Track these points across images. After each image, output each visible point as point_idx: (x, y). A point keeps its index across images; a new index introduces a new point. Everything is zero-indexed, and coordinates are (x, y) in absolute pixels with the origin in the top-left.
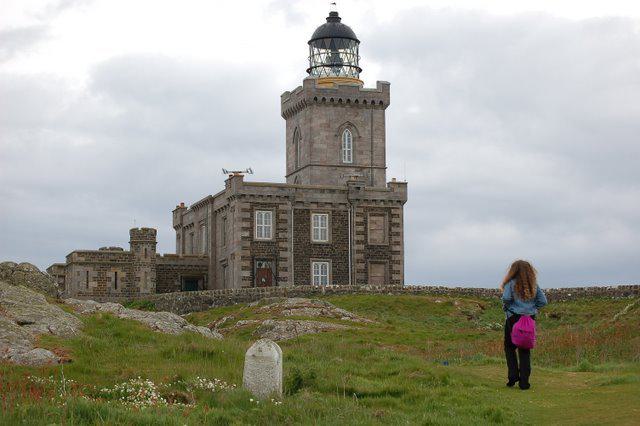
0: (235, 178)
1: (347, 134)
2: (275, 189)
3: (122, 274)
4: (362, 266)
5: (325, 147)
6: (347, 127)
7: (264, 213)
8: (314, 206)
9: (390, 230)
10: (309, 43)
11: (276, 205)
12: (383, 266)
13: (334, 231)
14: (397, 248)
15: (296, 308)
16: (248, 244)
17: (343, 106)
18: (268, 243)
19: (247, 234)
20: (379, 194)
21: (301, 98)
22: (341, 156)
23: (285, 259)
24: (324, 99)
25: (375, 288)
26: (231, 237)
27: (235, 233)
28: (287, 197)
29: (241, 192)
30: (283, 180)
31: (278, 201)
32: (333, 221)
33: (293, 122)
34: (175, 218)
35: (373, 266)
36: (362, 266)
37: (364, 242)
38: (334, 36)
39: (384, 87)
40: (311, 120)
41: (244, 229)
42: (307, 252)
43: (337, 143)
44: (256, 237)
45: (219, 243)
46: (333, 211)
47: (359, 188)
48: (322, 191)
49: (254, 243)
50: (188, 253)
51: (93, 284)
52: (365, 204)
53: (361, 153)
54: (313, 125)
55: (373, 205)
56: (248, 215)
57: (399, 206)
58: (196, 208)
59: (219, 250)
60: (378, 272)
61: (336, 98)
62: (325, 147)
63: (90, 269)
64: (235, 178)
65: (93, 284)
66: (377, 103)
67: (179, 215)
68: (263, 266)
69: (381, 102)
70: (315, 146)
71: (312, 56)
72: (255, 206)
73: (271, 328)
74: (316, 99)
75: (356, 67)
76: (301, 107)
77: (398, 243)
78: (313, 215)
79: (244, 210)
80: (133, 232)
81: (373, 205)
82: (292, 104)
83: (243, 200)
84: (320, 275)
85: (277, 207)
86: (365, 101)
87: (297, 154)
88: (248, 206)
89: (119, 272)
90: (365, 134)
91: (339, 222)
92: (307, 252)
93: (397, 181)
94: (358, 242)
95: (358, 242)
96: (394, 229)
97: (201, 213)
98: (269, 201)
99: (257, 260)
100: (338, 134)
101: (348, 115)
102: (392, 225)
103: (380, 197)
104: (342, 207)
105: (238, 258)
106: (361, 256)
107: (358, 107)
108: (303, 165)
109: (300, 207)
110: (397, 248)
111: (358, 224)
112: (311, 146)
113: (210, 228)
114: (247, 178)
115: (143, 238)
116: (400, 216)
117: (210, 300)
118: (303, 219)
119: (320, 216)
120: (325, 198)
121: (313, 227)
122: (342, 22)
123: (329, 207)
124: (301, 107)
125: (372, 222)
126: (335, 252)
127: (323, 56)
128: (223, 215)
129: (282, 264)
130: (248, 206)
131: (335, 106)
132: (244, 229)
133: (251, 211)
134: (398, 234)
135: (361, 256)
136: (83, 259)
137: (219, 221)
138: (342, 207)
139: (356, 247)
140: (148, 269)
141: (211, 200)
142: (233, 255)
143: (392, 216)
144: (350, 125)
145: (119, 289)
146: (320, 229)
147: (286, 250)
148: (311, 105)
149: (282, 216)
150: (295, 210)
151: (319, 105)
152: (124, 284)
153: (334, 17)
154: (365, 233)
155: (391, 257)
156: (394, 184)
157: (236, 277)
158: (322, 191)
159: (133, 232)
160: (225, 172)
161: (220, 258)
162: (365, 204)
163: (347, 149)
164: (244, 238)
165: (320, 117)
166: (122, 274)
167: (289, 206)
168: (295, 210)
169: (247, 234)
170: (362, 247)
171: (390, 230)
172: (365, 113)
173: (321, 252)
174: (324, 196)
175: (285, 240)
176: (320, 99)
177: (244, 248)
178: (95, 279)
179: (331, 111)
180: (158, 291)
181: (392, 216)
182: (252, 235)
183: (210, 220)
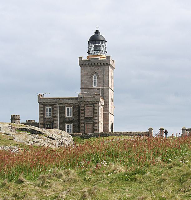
2: (52, 100)
4: (83, 125)
5: (86, 81)
9: (94, 111)
10: (88, 42)
11: (53, 105)
12: (91, 125)
14: (97, 118)
16: (43, 119)
20: (89, 99)
31: (53, 104)
36: (83, 125)
38: (96, 39)
43: (91, 80)
44: (46, 116)
47: (82, 97)
49: (44, 118)
52: (85, 103)
53: (100, 83)
55: (87, 103)
56: (43, 109)
60: (90, 126)
66: (105, 64)
69: (107, 63)
72: (45, 106)
77: (96, 116)
78: (66, 108)
81: (87, 103)
84: (69, 129)
86: (104, 63)
88: (43, 106)
91: (76, 109)
94: (82, 116)
95: (82, 116)
96: (95, 111)
98: (50, 104)
100: (91, 76)
102: (94, 110)
104: (77, 104)
107: (98, 66)
110: (97, 118)
111: (82, 110)
114: (45, 96)
118: (62, 109)
126: (74, 120)
133: (44, 108)
134: (97, 113)
138: (77, 104)
139: (57, 122)
143: (95, 106)
147: (56, 120)
149: (55, 109)
155: (94, 121)
162: (85, 103)
163: (95, 82)
169: (42, 116)
170: (84, 118)
171: (94, 111)
172: (102, 68)
173: (69, 120)
174: (69, 101)
175: (56, 117)
177: (41, 121)
181: (95, 106)
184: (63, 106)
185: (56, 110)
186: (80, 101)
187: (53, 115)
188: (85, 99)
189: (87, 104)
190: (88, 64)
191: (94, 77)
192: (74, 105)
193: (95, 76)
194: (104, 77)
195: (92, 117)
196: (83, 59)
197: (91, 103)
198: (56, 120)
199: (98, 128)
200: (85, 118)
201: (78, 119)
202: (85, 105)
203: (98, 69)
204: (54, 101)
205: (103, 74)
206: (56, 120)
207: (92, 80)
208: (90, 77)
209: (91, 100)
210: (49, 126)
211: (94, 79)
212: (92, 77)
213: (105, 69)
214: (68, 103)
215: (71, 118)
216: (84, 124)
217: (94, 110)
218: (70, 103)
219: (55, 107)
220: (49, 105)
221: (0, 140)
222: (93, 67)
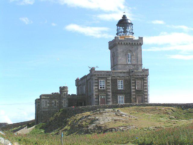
8: (118, 78)
9: (143, 85)
11: (106, 78)
14: (146, 91)
15: (108, 112)
20: (140, 73)
31: (106, 76)
39: (141, 39)
58: (81, 79)
60: (140, 98)
63: (47, 100)
64: (92, 70)
69: (140, 43)
73: (97, 120)
77: (146, 89)
81: (138, 77)
88: (97, 78)
92: (116, 93)
93: (145, 69)
97: (83, 81)
98: (104, 76)
106: (134, 93)
123: (123, 78)
126: (127, 93)
146: (120, 85)
153: (124, 17)
162: (135, 77)
172: (135, 47)
181: (144, 80)
184: (115, 79)
186: (132, 74)
187: (107, 87)
188: (136, 73)
189: (137, 78)
193: (129, 54)
195: (141, 89)
196: (79, 78)
197: (141, 77)
199: (147, 99)
201: (139, 101)
203: (132, 48)
204: (108, 74)
209: (141, 74)
210: (102, 97)
213: (138, 48)
215: (123, 90)
217: (144, 83)
219: (108, 80)
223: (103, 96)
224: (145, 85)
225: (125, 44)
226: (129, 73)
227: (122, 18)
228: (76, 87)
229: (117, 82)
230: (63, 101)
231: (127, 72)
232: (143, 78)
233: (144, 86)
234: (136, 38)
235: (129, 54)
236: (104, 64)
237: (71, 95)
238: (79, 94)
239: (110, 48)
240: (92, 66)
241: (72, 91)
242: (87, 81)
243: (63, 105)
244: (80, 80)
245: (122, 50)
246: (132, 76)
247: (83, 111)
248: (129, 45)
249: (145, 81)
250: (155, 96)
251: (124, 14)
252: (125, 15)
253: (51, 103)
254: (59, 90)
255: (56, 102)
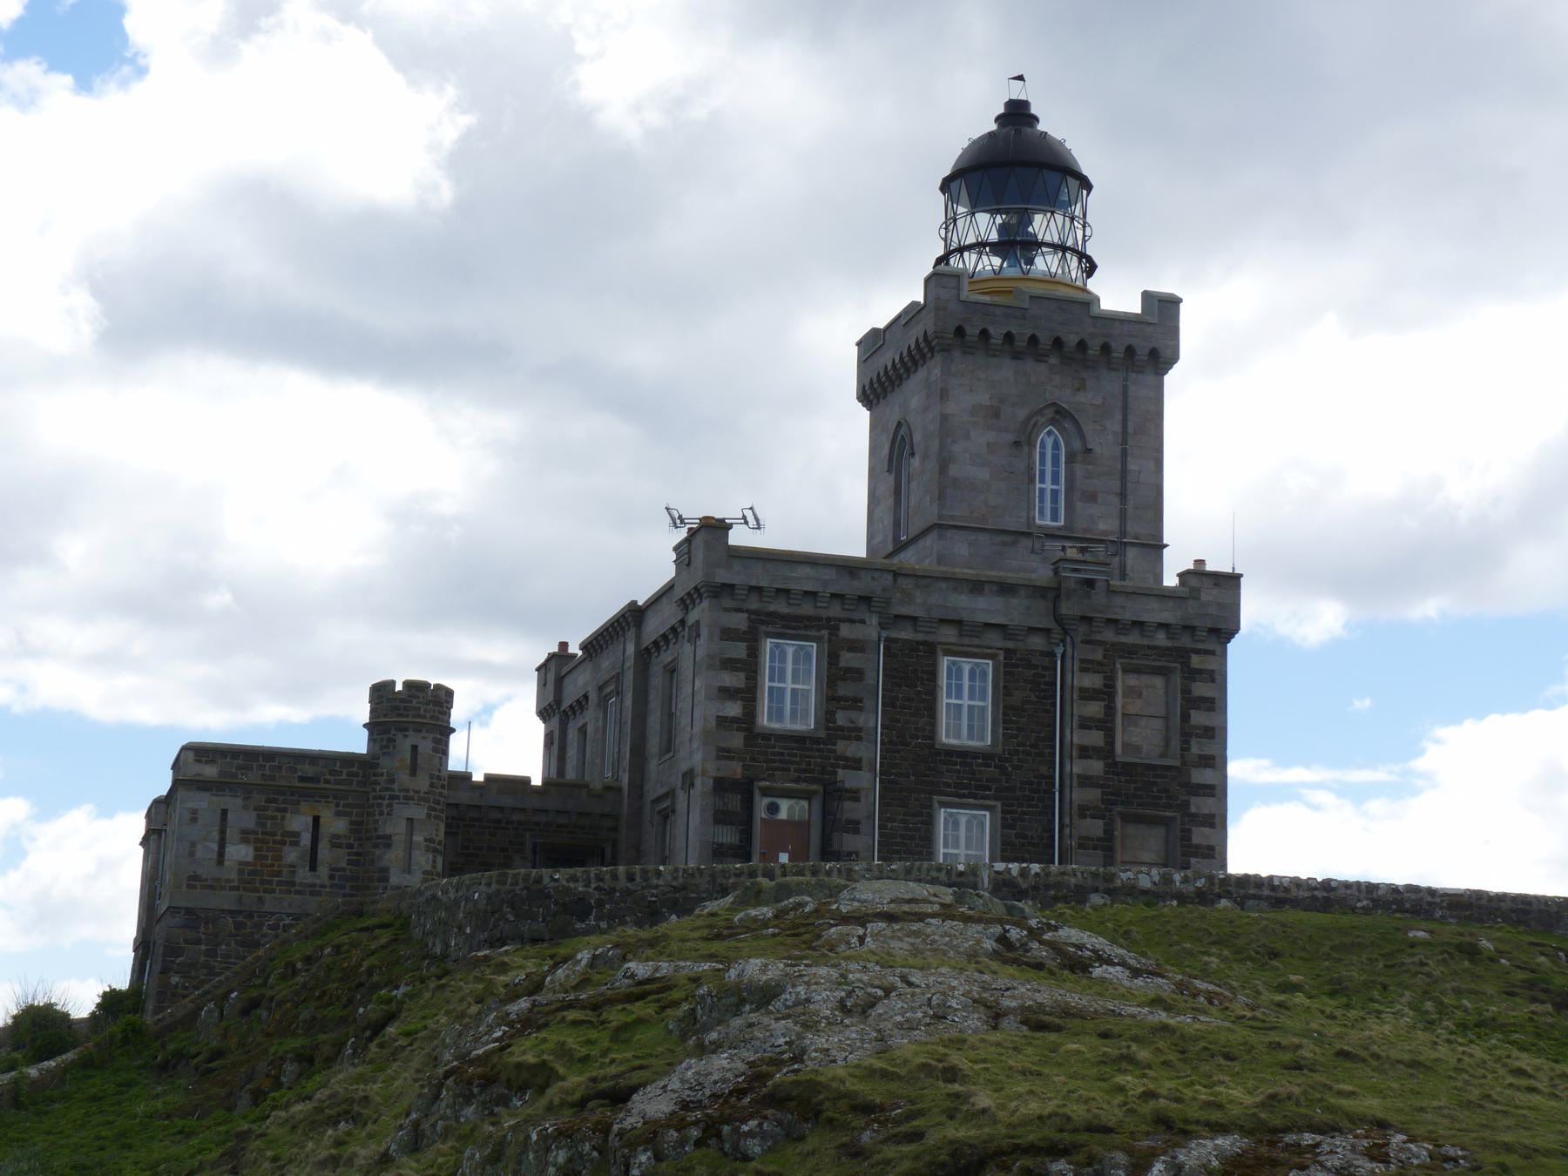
0: (706, 538)
1: (1048, 439)
2: (829, 574)
3: (336, 825)
4: (1095, 827)
5: (983, 474)
6: (1053, 422)
7: (790, 647)
8: (948, 634)
9: (1185, 717)
11: (832, 625)
12: (1160, 832)
13: (1008, 713)
15: (890, 918)
16: (737, 740)
17: (1040, 357)
18: (798, 739)
19: (734, 709)
20: (1154, 604)
21: (917, 332)
22: (1030, 507)
23: (855, 795)
24: (984, 334)
25: (1167, 880)
26: (685, 721)
27: (698, 705)
28: (866, 600)
29: (723, 576)
30: (856, 547)
31: (835, 611)
32: (1004, 689)
33: (893, 413)
34: (542, 684)
35: (1131, 829)
36: (1095, 827)
37: (1106, 752)
39: (1163, 308)
40: (944, 395)
41: (727, 693)
42: (927, 772)
44: (764, 721)
45: (654, 743)
46: (1009, 652)
47: (1090, 583)
48: (976, 587)
50: (571, 775)
51: (239, 852)
52: (1109, 635)
53: (1092, 497)
54: (951, 408)
56: (739, 650)
57: (1211, 645)
58: (594, 646)
59: (653, 765)
61: (1022, 331)
62: (983, 474)
63: (233, 803)
64: (706, 538)
65: (239, 852)
67: (551, 677)
68: (783, 815)
70: (954, 471)
71: (951, 221)
72: (761, 624)
73: (765, 996)
74: (960, 331)
75: (1082, 255)
76: (913, 361)
78: (945, 662)
79: (728, 634)
80: (381, 693)
81: (1133, 638)
82: (887, 358)
83: (727, 602)
85: (834, 630)
87: (897, 503)
88: (739, 621)
89: (327, 815)
90: (1104, 445)
91: (1026, 693)
92: (927, 772)
93: (1209, 567)
94: (1085, 752)
95: (1085, 752)
97: (607, 663)
98: (807, 609)
99: (766, 792)
100: (1023, 441)
101: (1059, 389)
103: (1155, 613)
104: (1037, 642)
105: (702, 785)
106: (1092, 795)
108: (917, 525)
109: (906, 634)
111: (1087, 695)
112: (943, 468)
113: (628, 702)
114: (739, 537)
115: (393, 683)
116: (1217, 678)
117: (582, 899)
119: (966, 665)
120: (986, 608)
121: (944, 701)
122: (1041, 127)
123: (994, 639)
124: (913, 361)
125: (1132, 692)
126: (1012, 782)
127: (986, 225)
128: (666, 657)
129: (849, 810)
130: (739, 621)
131: (1017, 356)
132: (727, 693)
133: (752, 640)
135: (1092, 795)
136: (210, 771)
137: (657, 680)
138: (1037, 642)
140: (419, 813)
141: (633, 615)
142: (689, 776)
143: (1193, 674)
144: (1061, 415)
145: (323, 871)
146: (965, 707)
148: (946, 349)
149: (848, 659)
150: (888, 640)
151: (968, 349)
152: (342, 858)
153: (1017, 115)
154: (1105, 724)
155: (1187, 804)
156: (1197, 576)
157: (692, 832)
158: (976, 587)
159: (381, 693)
160: (677, 521)
161: (653, 790)
162: (1109, 635)
163: (1048, 486)
164: (723, 722)
165: (971, 388)
166: (336, 825)
167: (870, 630)
168: (888, 640)
169: (734, 709)
170: (1096, 767)
171: (1185, 717)
173: (967, 777)
175: (855, 733)
176: (972, 331)
177: (724, 754)
178: (245, 835)
179: (1005, 372)
180: (452, 869)
181: (1193, 674)
182: (750, 713)
183: (629, 677)
184: (913, 647)
185: (857, 674)
188: (1119, 601)
189: (1130, 651)
190: (1009, 337)
191: (1043, 446)
192: (1010, 645)
194: (1124, 454)
197: (1161, 639)
198: (1084, 811)
200: (1113, 766)
201: (1044, 770)
202: (1113, 650)
205: (1118, 428)
206: (855, 764)
207: (1031, 468)
208: (1017, 444)
211: (1043, 463)
212: (1031, 444)
214: (965, 616)
216: (1100, 823)
218: (987, 625)
220: (796, 618)
221: (515, 1172)
222: (1042, 367)
223: (788, 794)
224: (1198, 718)
225: (1020, 360)
226: (1051, 593)
227: (994, 127)
228: (538, 729)
229: (933, 675)
230: (395, 827)
231: (1038, 591)
232: (1183, 654)
233: (1187, 735)
234: (1117, 293)
235: (1049, 442)
236: (816, 491)
237: (478, 777)
238: (561, 772)
239: (870, 394)
240: (695, 511)
241: (500, 739)
242: (645, 656)
243: (393, 857)
244: (582, 661)
245: (983, 398)
246: (1083, 628)
247: (583, 916)
248: (1053, 360)
249: (1201, 689)
250: (1285, 823)
251: (1017, 92)
252: (1022, 97)
253: (267, 839)
254: (363, 712)
255: (323, 830)
